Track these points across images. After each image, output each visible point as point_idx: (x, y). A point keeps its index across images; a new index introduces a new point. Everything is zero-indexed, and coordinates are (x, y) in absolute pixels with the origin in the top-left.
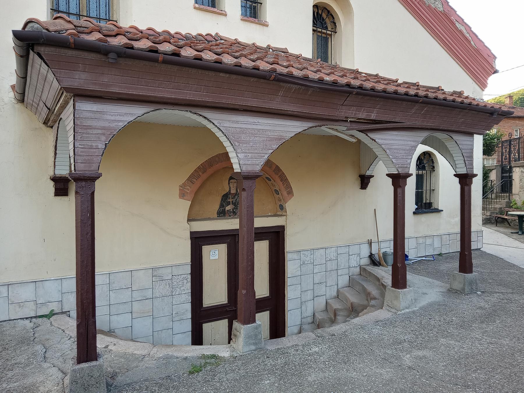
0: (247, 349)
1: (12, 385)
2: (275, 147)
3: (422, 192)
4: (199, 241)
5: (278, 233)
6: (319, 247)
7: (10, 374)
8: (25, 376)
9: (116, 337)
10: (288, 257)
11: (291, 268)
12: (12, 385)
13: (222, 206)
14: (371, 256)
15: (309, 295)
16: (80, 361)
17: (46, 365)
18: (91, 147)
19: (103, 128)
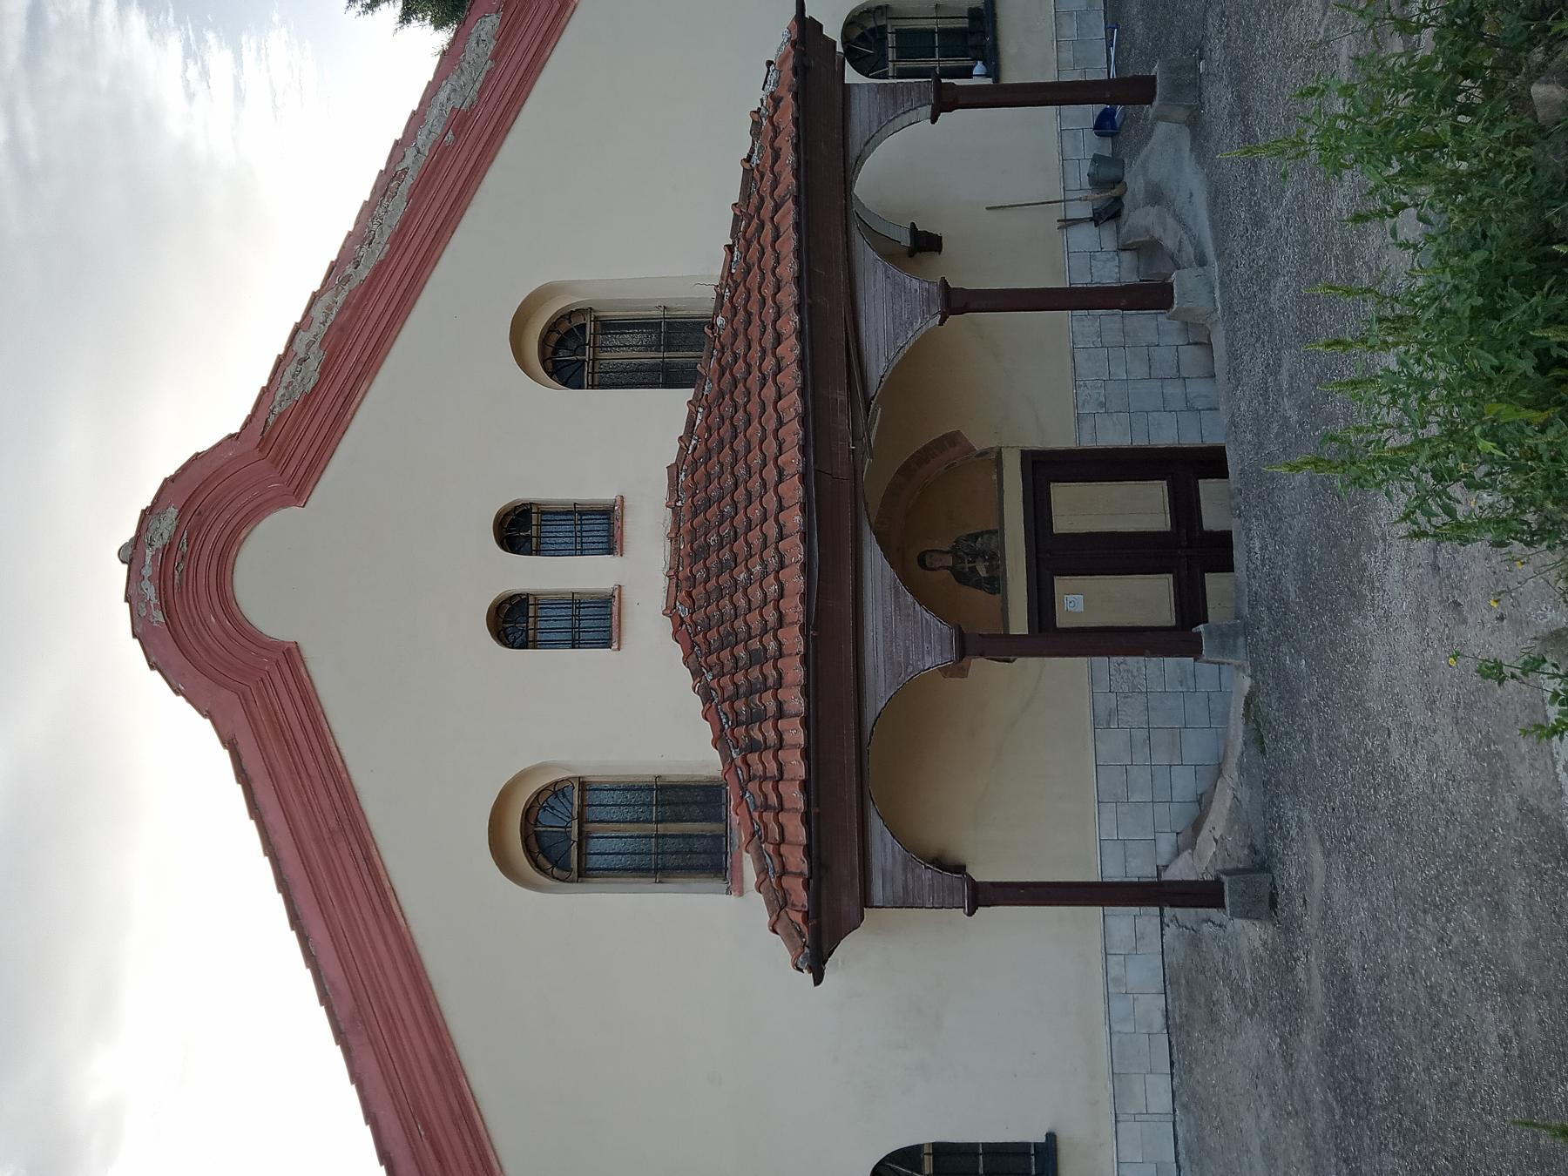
0: (1242, 652)
1: (1248, 977)
2: (910, 598)
3: (943, 32)
4: (1048, 636)
5: (1034, 463)
6: (1070, 365)
7: (1234, 974)
8: (1239, 957)
9: (1225, 756)
10: (1087, 443)
11: (1113, 435)
12: (1248, 977)
13: (978, 584)
14: (1097, 219)
15: (1174, 389)
16: (1219, 904)
17: (1230, 928)
18: (931, 886)
19: (905, 870)
